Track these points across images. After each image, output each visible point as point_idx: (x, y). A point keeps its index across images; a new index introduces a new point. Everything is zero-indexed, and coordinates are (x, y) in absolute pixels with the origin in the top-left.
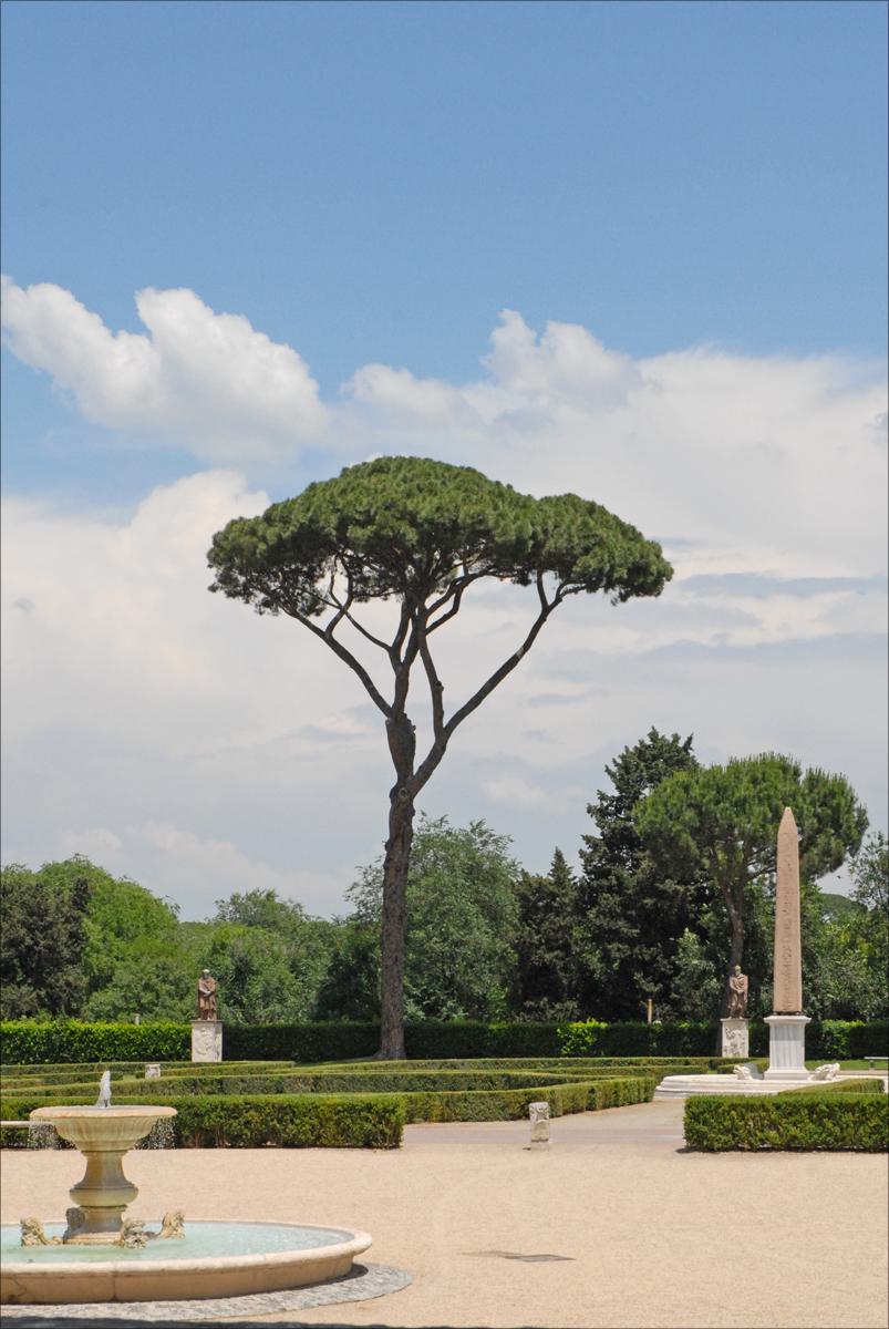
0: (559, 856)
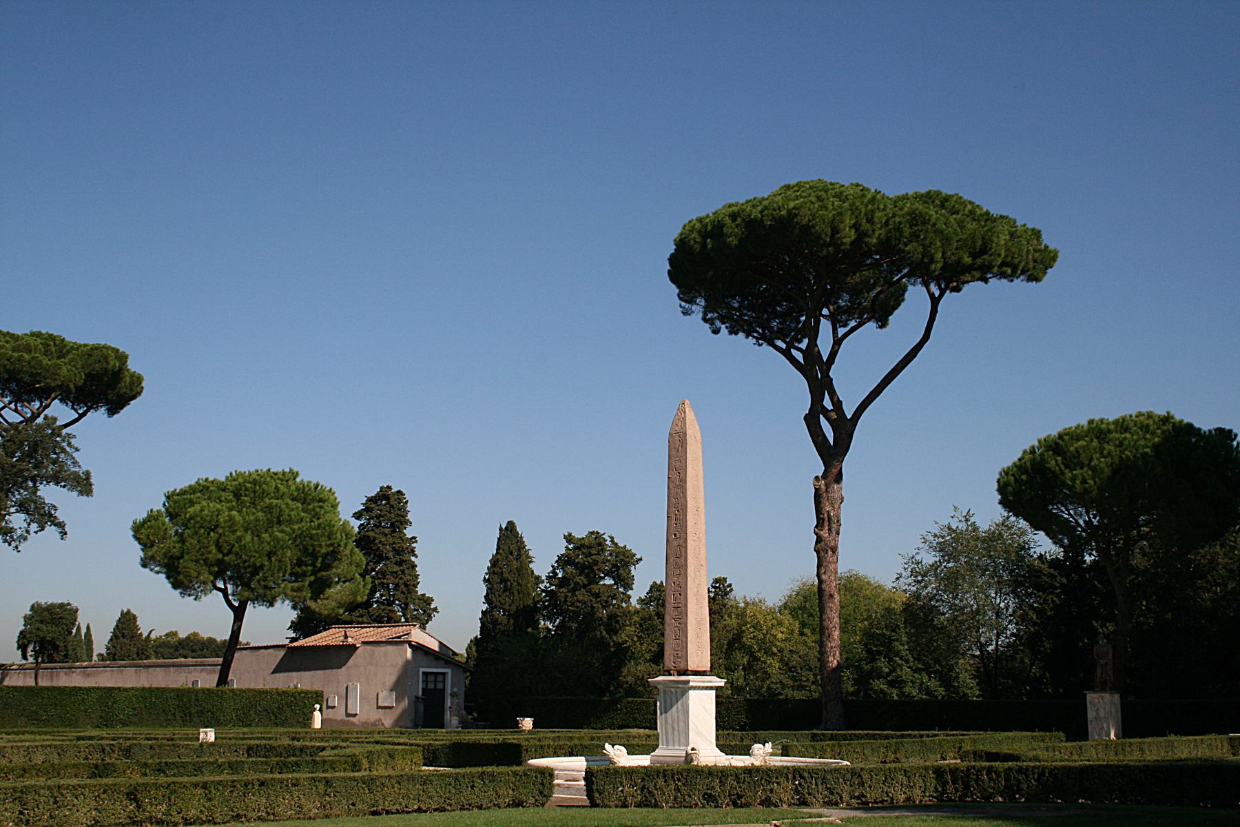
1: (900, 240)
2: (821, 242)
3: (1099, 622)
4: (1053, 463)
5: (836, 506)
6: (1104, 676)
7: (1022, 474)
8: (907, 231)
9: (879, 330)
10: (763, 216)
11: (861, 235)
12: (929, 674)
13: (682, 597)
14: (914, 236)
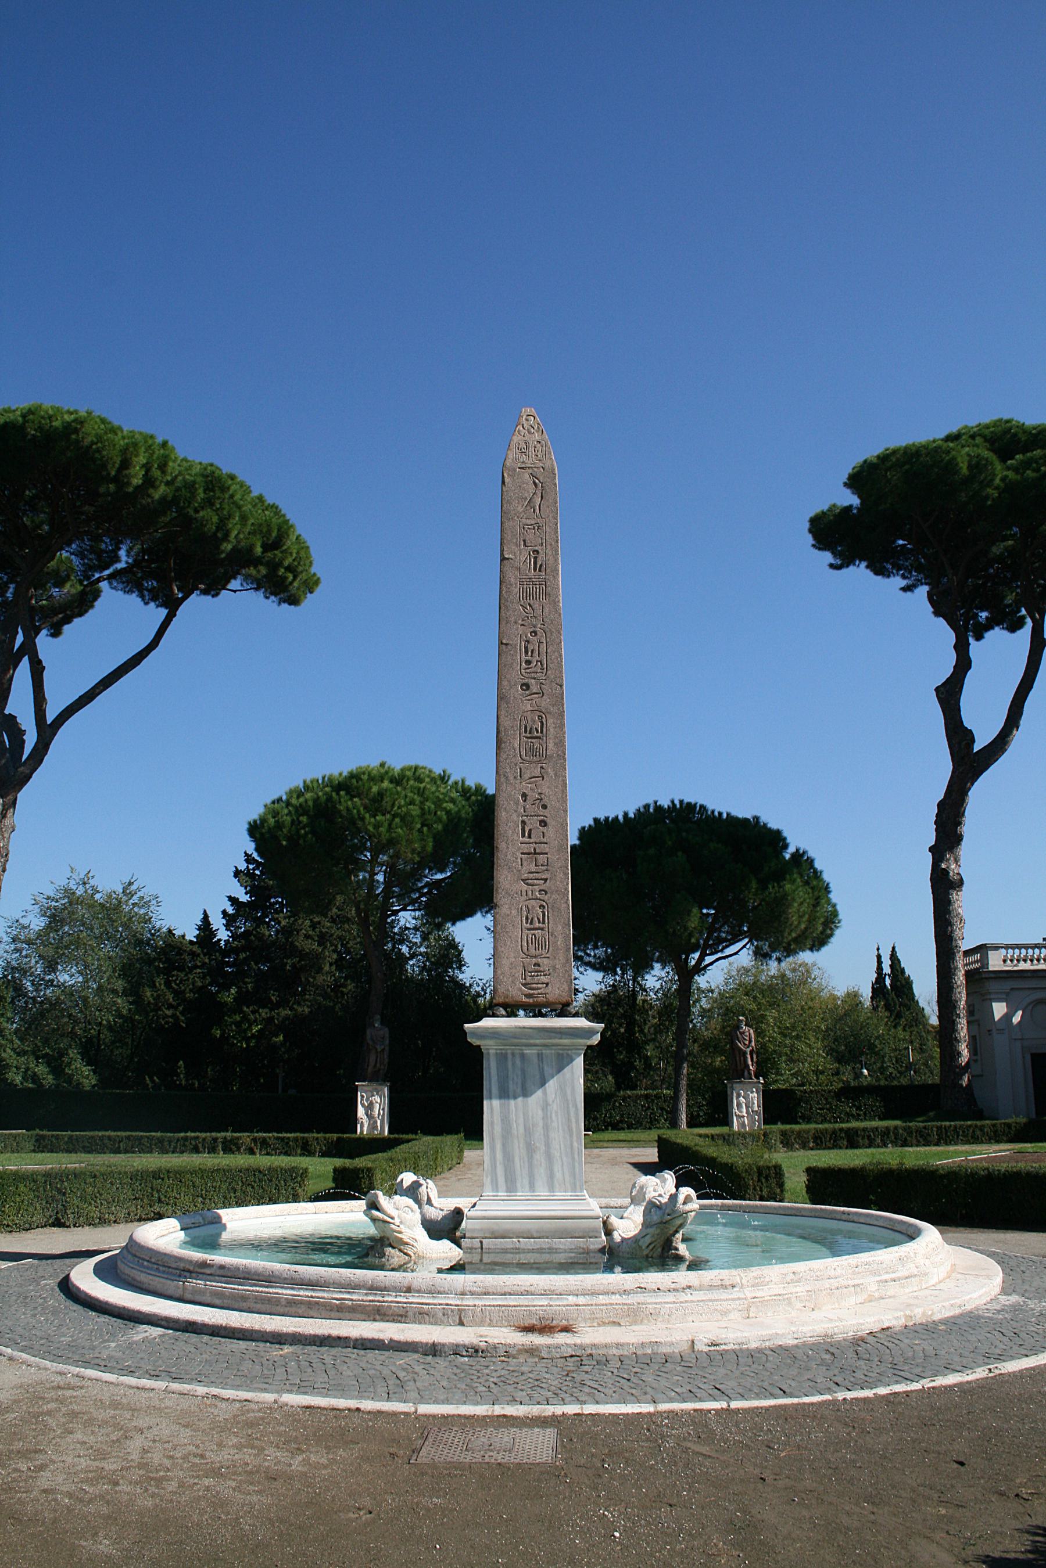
0: (206, 917)
1: (190, 503)
2: (104, 473)
3: (251, 1008)
4: (345, 803)
5: (6, 835)
6: (378, 1065)
7: (302, 815)
8: (201, 495)
9: (50, 638)
10: (25, 421)
11: (149, 482)
12: (37, 1058)
13: (550, 831)
14: (209, 503)
